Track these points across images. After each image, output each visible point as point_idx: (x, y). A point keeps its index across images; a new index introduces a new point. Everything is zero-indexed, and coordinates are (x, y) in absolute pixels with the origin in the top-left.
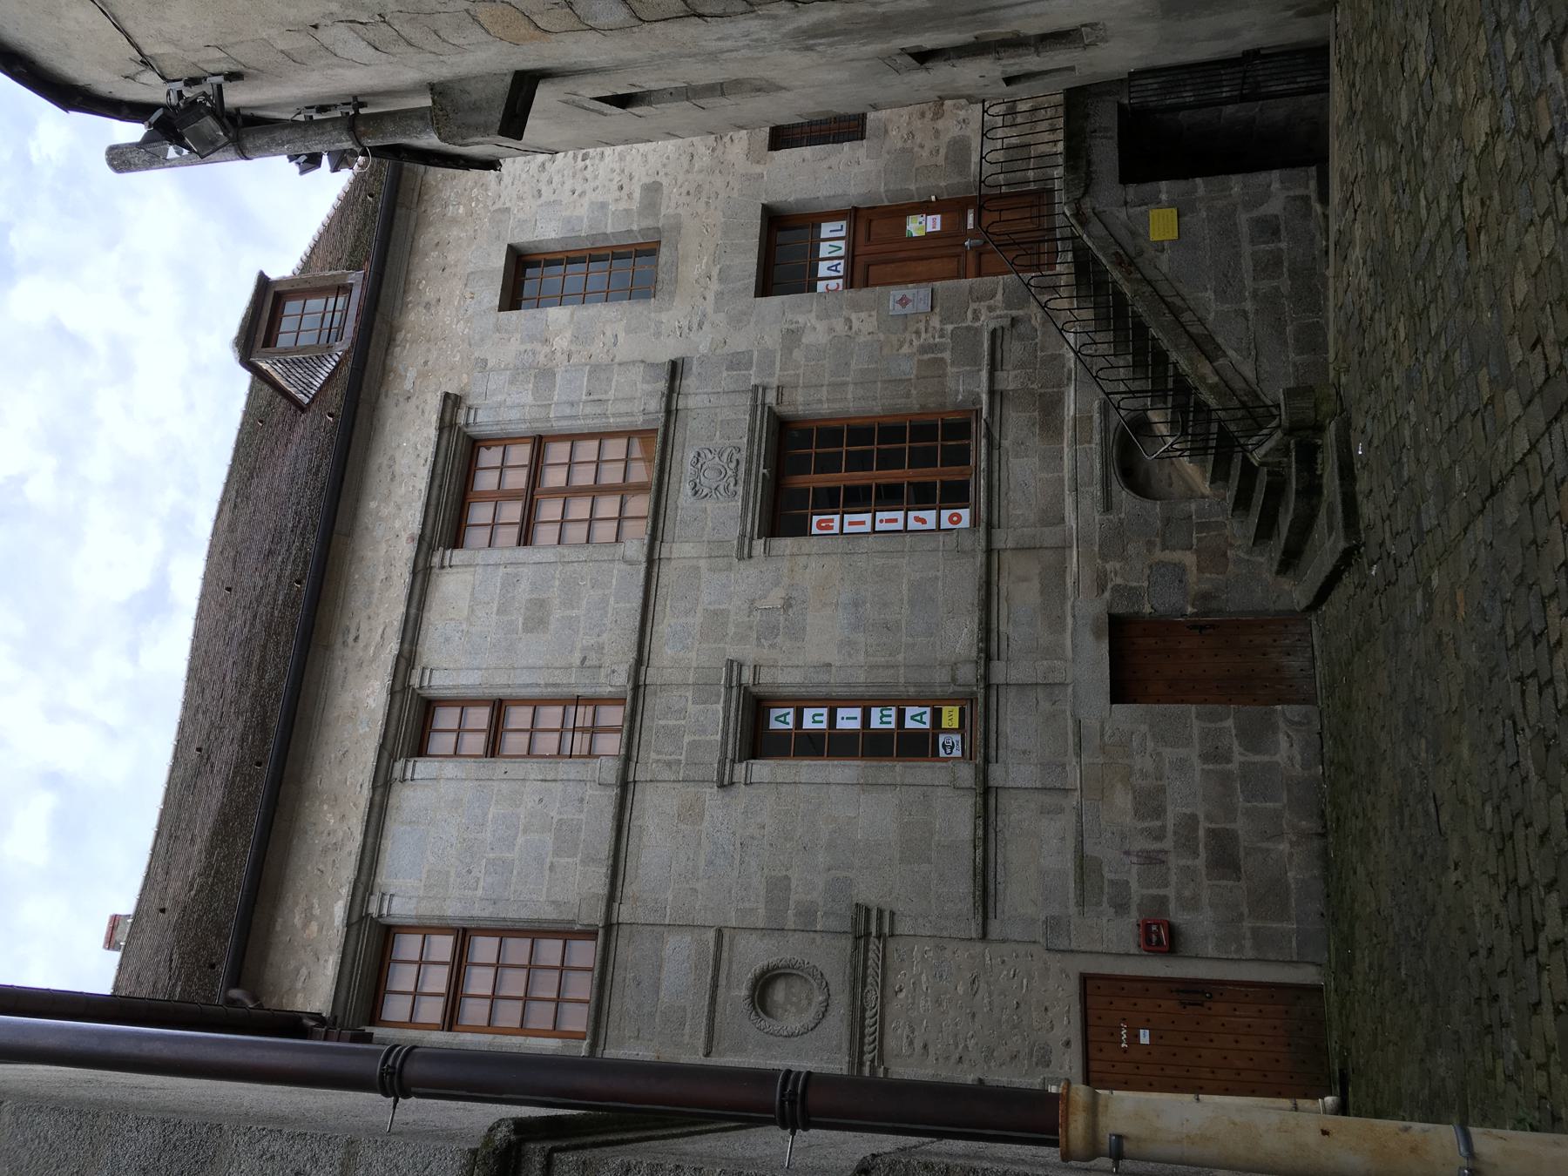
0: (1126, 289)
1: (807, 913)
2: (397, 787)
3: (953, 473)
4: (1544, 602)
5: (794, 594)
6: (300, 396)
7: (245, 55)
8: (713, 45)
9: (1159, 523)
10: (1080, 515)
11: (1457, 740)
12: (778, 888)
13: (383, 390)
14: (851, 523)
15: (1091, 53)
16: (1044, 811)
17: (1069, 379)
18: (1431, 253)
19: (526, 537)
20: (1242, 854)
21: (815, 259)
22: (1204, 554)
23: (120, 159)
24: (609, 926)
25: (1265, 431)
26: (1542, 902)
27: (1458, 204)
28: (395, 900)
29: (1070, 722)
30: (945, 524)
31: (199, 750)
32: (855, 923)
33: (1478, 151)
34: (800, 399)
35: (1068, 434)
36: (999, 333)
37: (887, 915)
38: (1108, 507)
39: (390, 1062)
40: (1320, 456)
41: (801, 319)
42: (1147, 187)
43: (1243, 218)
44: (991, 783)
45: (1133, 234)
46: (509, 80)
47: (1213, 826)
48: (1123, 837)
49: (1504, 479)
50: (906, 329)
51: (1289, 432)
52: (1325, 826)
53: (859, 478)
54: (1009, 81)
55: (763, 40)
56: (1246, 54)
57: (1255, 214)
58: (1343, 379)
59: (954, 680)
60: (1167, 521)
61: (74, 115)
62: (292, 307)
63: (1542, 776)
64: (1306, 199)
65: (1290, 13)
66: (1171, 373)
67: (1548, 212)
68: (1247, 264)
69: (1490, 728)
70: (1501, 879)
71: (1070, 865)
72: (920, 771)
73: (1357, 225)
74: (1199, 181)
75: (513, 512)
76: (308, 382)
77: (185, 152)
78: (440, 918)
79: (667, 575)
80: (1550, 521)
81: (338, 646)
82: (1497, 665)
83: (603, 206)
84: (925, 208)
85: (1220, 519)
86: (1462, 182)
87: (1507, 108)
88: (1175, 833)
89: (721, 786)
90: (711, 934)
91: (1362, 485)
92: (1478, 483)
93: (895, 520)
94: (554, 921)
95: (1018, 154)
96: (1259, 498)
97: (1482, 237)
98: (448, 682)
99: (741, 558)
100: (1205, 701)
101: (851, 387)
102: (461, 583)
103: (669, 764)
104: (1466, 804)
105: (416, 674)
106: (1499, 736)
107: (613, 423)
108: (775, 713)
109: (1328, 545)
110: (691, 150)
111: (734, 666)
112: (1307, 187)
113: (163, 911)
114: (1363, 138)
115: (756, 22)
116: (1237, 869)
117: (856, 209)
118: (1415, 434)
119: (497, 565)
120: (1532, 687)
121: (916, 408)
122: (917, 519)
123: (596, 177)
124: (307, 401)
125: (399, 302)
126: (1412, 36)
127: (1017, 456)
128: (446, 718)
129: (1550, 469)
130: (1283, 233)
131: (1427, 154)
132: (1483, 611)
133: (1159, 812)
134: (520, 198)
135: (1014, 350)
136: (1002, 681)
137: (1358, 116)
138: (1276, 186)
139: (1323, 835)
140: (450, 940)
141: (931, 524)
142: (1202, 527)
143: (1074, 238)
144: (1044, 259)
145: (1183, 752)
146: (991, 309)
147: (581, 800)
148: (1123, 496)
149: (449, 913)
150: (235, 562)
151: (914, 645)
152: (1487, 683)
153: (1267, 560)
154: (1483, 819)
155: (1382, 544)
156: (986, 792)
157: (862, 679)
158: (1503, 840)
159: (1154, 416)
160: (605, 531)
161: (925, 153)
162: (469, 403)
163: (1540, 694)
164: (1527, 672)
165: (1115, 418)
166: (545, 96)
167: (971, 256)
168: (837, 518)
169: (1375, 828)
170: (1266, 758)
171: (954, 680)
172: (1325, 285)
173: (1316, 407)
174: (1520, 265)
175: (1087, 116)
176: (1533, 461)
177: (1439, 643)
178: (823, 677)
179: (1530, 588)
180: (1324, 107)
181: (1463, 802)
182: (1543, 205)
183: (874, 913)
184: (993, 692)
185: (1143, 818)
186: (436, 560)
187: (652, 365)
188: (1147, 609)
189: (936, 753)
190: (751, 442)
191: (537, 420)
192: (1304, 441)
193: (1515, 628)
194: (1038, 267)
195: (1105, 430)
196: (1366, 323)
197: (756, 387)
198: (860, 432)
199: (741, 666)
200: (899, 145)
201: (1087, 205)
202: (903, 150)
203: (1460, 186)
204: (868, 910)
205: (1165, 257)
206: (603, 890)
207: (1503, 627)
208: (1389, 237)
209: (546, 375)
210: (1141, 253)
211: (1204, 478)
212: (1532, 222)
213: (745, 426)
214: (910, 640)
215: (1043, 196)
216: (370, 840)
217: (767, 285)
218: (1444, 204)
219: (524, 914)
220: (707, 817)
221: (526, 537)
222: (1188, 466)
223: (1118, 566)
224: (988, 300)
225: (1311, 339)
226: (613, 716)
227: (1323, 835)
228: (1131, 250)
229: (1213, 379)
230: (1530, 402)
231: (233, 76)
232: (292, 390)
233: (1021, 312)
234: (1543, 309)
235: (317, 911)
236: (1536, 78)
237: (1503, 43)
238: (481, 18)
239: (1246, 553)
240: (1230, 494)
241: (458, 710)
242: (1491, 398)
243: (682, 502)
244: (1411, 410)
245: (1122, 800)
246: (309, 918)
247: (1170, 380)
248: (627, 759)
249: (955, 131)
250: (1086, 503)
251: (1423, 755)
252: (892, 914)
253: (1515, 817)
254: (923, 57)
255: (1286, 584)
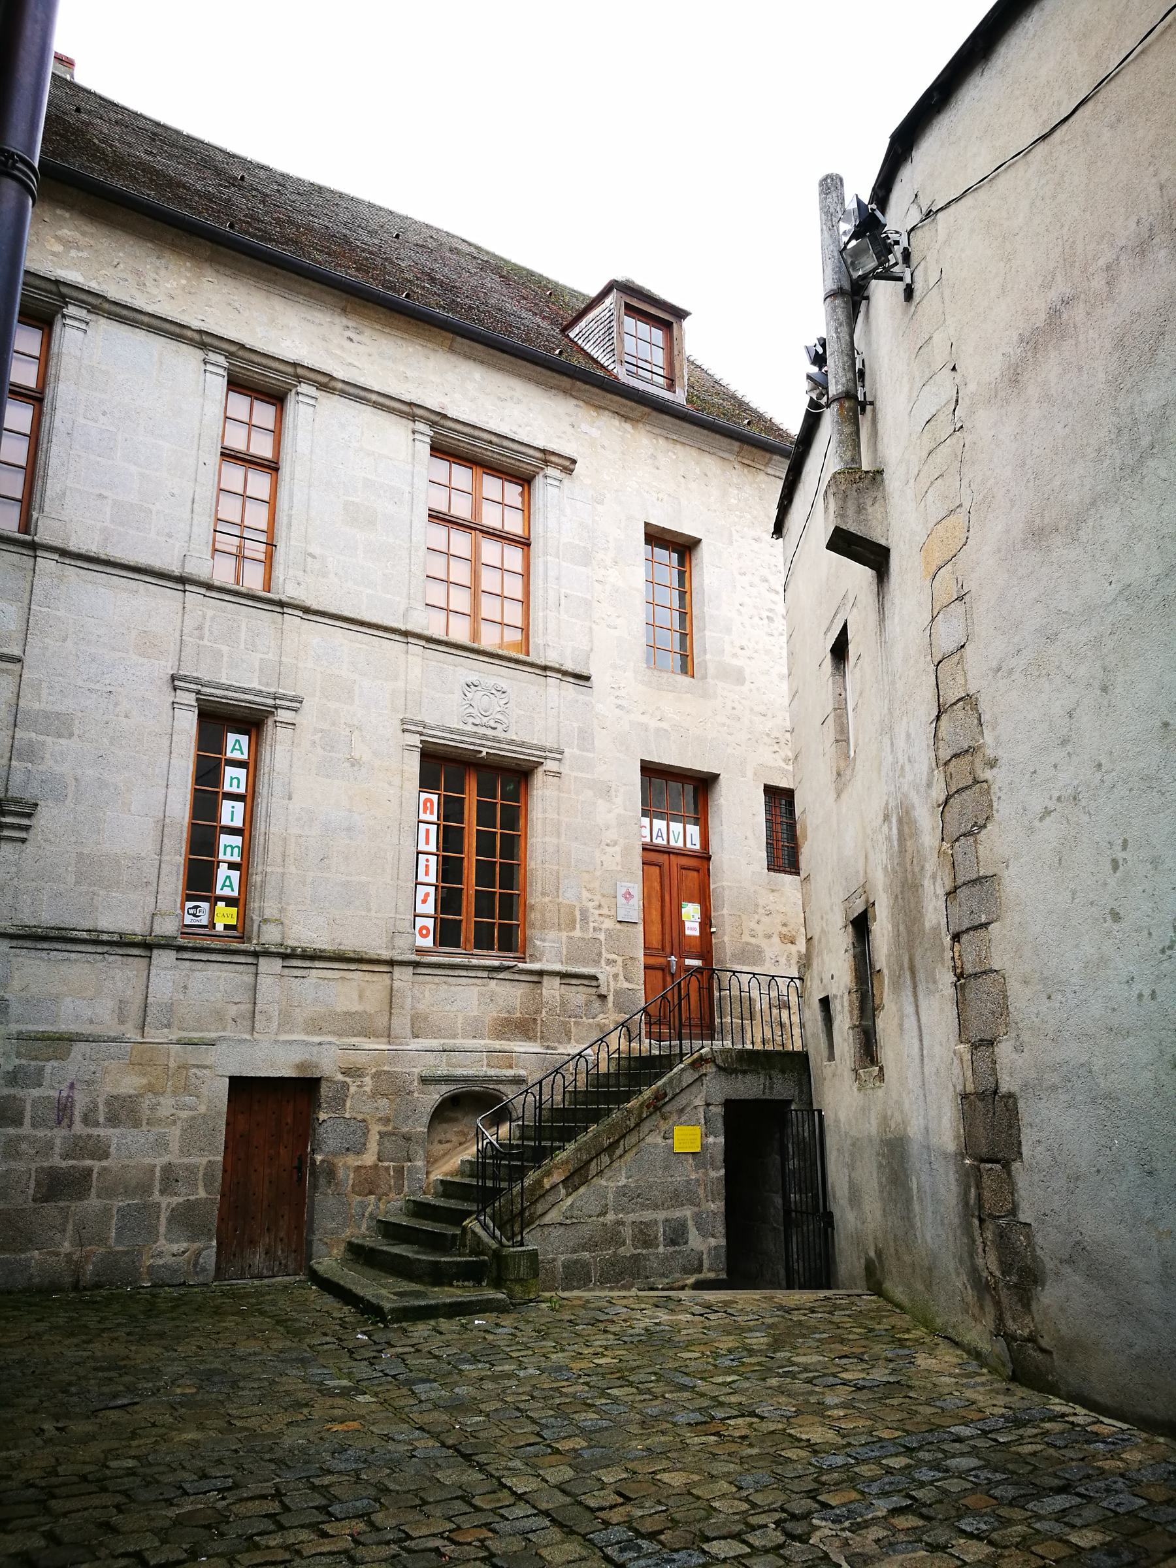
0: (633, 1103)
1: (31, 753)
2: (199, 354)
3: (468, 932)
4: (365, 1516)
5: (364, 770)
6: (577, 330)
7: (928, 302)
8: (900, 729)
9: (405, 1130)
10: (420, 1056)
11: (201, 1427)
12: (60, 725)
13: (581, 404)
14: (428, 831)
15: (848, 1076)
16: (122, 1004)
17: (548, 1047)
18: (684, 1388)
19: (435, 517)
20: (61, 1204)
21: (669, 817)
22: (375, 1167)
23: (831, 185)
24: (33, 546)
25: (498, 1233)
26: (32, 1528)
27: (736, 1413)
28: (80, 334)
29: (213, 1035)
30: (420, 922)
31: (242, 178)
32: (17, 801)
33: (792, 1431)
34: (548, 793)
35: (498, 1044)
36: (594, 983)
37: (23, 835)
38: (425, 1080)
39: (19, 165)
40: (471, 1284)
41: (619, 800)
42: (720, 1125)
43: (687, 1212)
44: (155, 952)
45: (681, 1111)
46: (883, 542)
47: (95, 1175)
48: (89, 1083)
49: (481, 1467)
50: (603, 896)
51: (497, 1255)
52: (85, 1289)
53: (471, 842)
54: (825, 1002)
55: (902, 775)
56: (830, 1215)
57: (690, 1223)
58: (543, 1305)
59: (266, 921)
60: (407, 1138)
61: (888, 141)
62: (658, 335)
63: (178, 1522)
64: (699, 1270)
65: (872, 1254)
66: (557, 1144)
67: (754, 1505)
68: (648, 1215)
69: (220, 1462)
70: (54, 1480)
71: (63, 1027)
72: (174, 880)
73: (689, 1317)
74: (722, 1172)
75: (461, 508)
76: (588, 335)
77: (845, 239)
78: (57, 378)
79: (393, 648)
80: (449, 1519)
81: (345, 321)
82: (289, 1467)
83: (728, 630)
84: (706, 921)
85: (406, 1189)
86: (757, 1416)
87: (840, 1460)
88: (90, 1136)
89: (173, 678)
90: (16, 651)
91: (444, 1324)
92: (472, 1440)
93: (427, 874)
94: (43, 492)
95: (748, 1010)
96: (428, 1226)
97: (713, 1438)
98: (301, 420)
99: (403, 721)
100: (225, 1171)
101: (554, 840)
102: (402, 449)
103: (200, 628)
104: (132, 1438)
105: (312, 391)
106: (214, 1472)
107: (537, 614)
108: (244, 739)
109: (384, 1292)
110: (770, 715)
111: (296, 703)
112: (709, 1270)
113: (78, 110)
114: (769, 1321)
115: (925, 769)
116: (46, 1199)
117: (709, 858)
118: (509, 1376)
119: (412, 485)
120: (273, 1507)
121: (531, 901)
122: (427, 895)
123: (753, 627)
124: (572, 335)
125: (657, 431)
126: (873, 1366)
127: (481, 994)
128: (264, 414)
129: (502, 1516)
130: (671, 1249)
131: (774, 1382)
132: (343, 1451)
133: (113, 1120)
134: (740, 556)
135: (578, 996)
136: (261, 969)
137: (787, 1316)
138: (713, 1242)
139: (76, 1287)
140: (32, 383)
141: (420, 909)
142: (400, 1171)
143: (682, 1055)
144: (655, 1029)
145: (175, 1146)
146: (616, 976)
147: (170, 536)
148: (435, 1095)
149: (62, 386)
150: (423, 246)
151: (304, 883)
152: (267, 1456)
153: (362, 1232)
154: (117, 1457)
155: (390, 1345)
156: (148, 946)
157: (272, 830)
158: (98, 1480)
159: (504, 1130)
160: (437, 594)
161: (753, 925)
162: (566, 481)
163: (265, 1516)
164: (287, 1500)
165: (509, 1091)
166: (860, 574)
167: (662, 961)
168: (434, 818)
169: (89, 1342)
170: (162, 1229)
171: (266, 921)
172: (624, 1288)
173: (519, 1281)
174: (696, 1478)
175: (783, 1072)
176: (505, 1497)
177: (299, 1405)
178: (278, 789)
179: (377, 1500)
180: (776, 1286)
181: (134, 1435)
182: (758, 1499)
183: (26, 822)
184: (250, 960)
185: (108, 1103)
186: (420, 426)
187: (588, 657)
188: (322, 1116)
189: (189, 898)
190: (512, 742)
191: (545, 545)
192: (491, 1269)
193: (331, 1485)
194: (649, 1023)
195: (499, 1081)
196: (602, 1326)
197: (562, 753)
198: (512, 846)
199: (296, 710)
200: (761, 902)
201: (710, 1069)
202: (757, 905)
203: (753, 1414)
204: (29, 816)
205: (659, 1140)
206: (72, 546)
207: (329, 1472)
208: (688, 1345)
209: (586, 559)
210: (664, 1118)
211: (446, 1174)
212: (740, 1488)
213: (526, 739)
214: (309, 880)
215: (709, 1030)
216: (146, 319)
217: (651, 771)
218: (733, 1399)
219: (54, 462)
220: (141, 660)
221: (435, 517)
222: (470, 1152)
223: (367, 1089)
224: (625, 975)
225: (576, 1275)
226: (253, 579)
227: (76, 1287)
228: (667, 1108)
229: (547, 1183)
230: (563, 1491)
231: (909, 293)
232: (583, 324)
233: (610, 1005)
234: (659, 1503)
235: (73, 253)
236: (874, 1489)
237: (896, 1455)
238: (952, 518)
239: (371, 1214)
240: (429, 1198)
241: (271, 427)
242: (557, 1452)
243: (461, 671)
244: (531, 1371)
245: (130, 1083)
246: (67, 244)
247: (548, 1144)
248: (209, 587)
249: (769, 953)
250: (430, 1058)
251: (179, 1391)
252: (24, 841)
253: (125, 1493)
254: (861, 925)
255: (338, 1251)
